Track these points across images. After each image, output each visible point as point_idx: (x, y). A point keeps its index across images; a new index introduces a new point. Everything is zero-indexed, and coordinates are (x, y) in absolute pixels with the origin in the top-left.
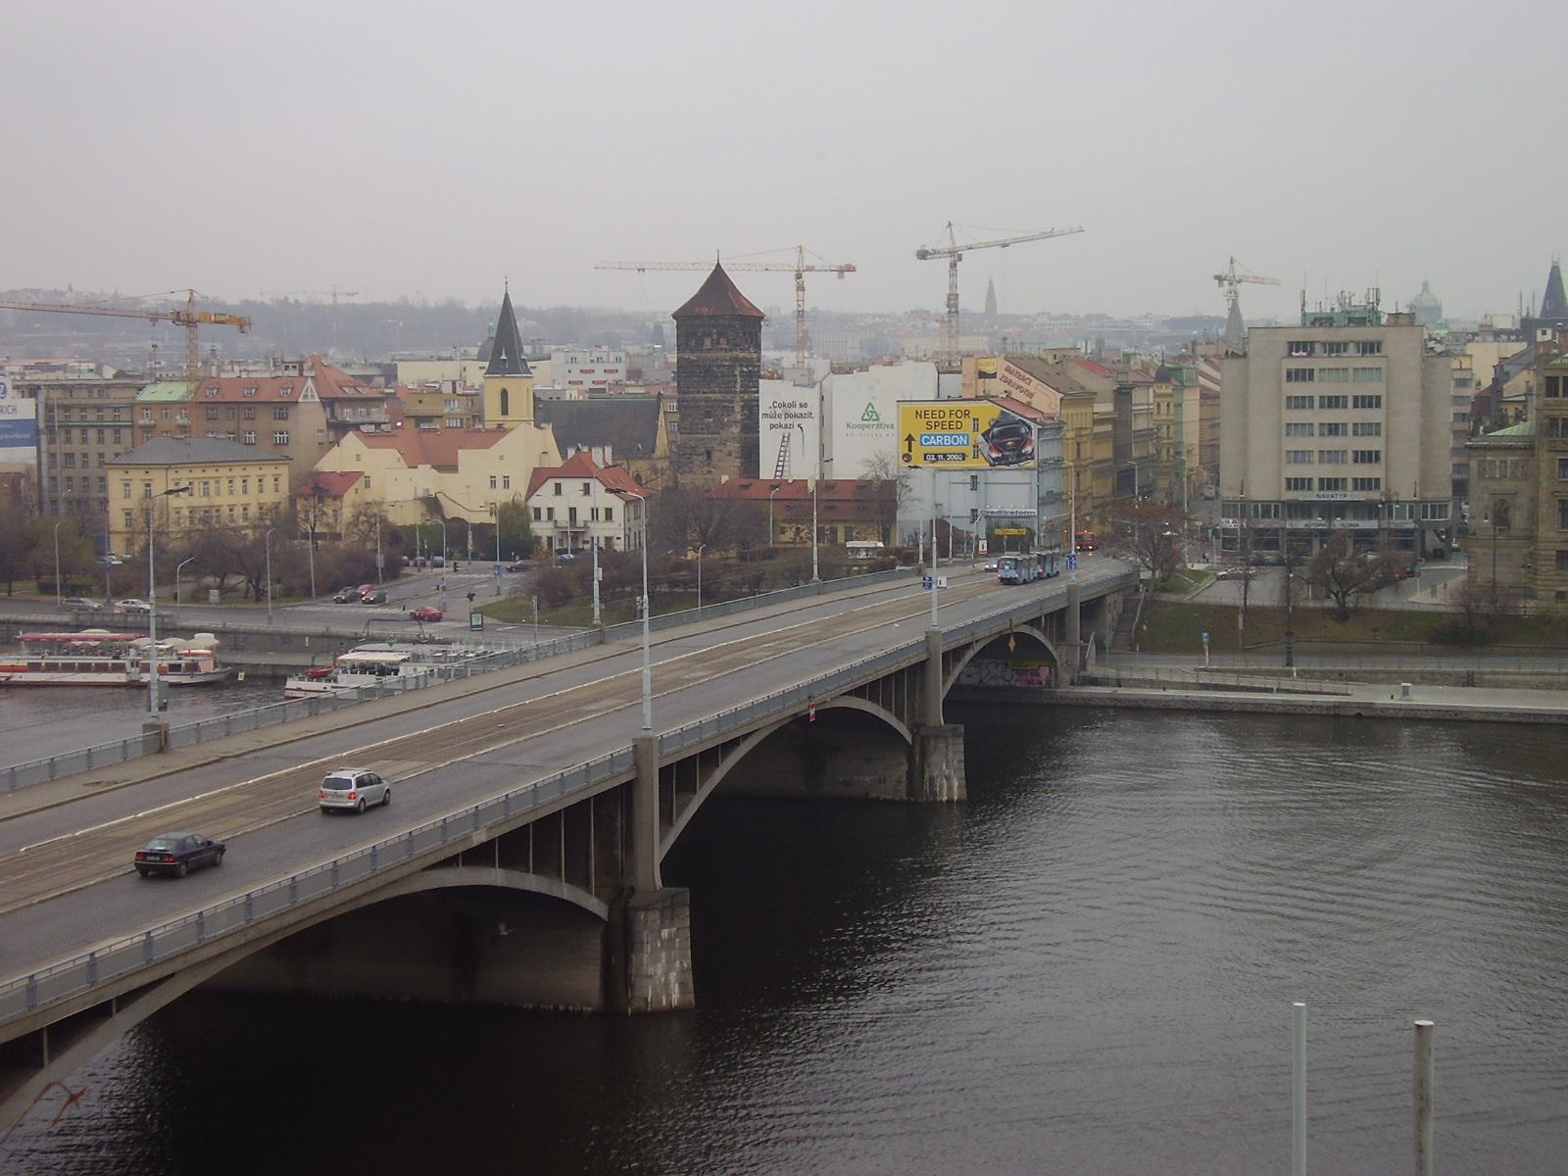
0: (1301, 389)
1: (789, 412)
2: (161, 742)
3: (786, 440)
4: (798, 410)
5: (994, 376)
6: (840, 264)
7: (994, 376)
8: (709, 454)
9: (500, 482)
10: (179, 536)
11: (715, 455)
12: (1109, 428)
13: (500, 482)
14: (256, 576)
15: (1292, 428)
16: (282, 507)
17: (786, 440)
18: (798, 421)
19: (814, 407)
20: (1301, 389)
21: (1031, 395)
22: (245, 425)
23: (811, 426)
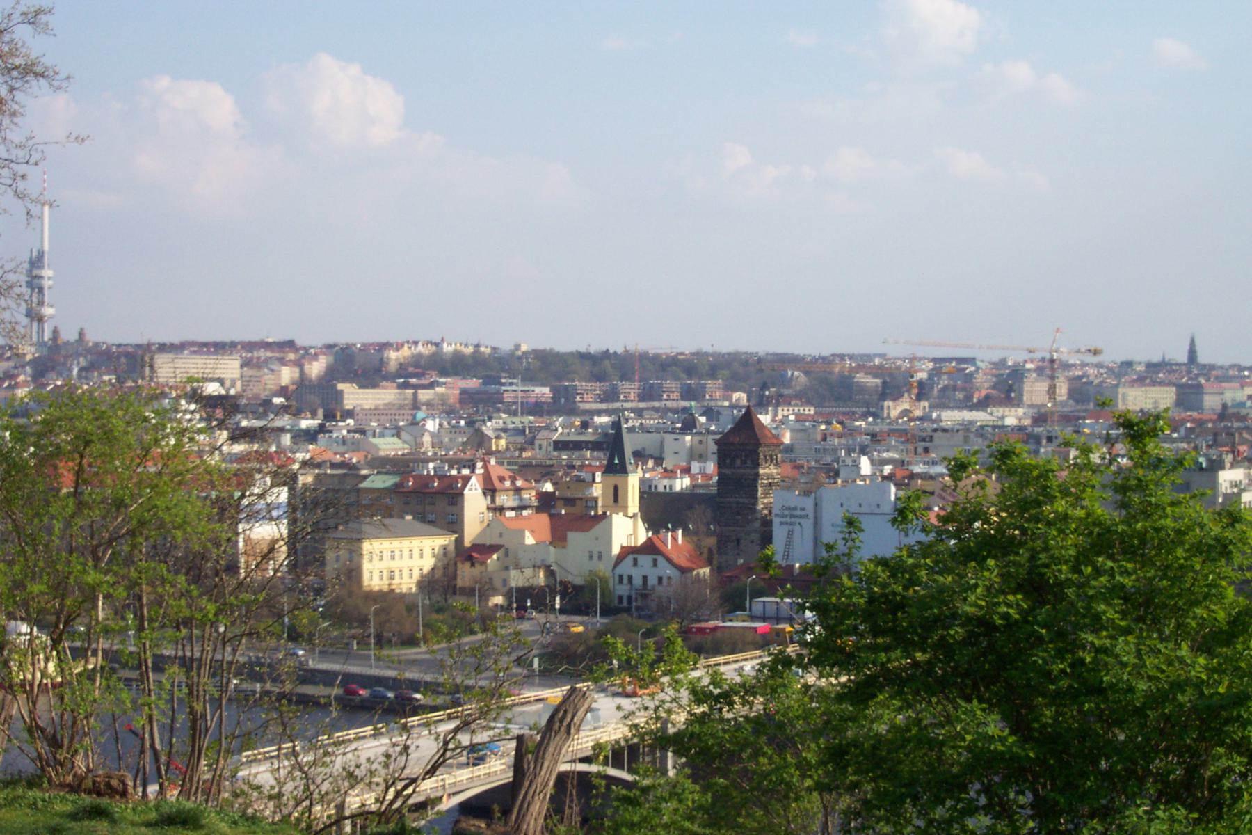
3: (790, 533)
4: (798, 512)
7: (932, 493)
8: (738, 541)
9: (595, 557)
13: (595, 557)
17: (790, 533)
18: (798, 520)
22: (428, 508)
23: (808, 524)
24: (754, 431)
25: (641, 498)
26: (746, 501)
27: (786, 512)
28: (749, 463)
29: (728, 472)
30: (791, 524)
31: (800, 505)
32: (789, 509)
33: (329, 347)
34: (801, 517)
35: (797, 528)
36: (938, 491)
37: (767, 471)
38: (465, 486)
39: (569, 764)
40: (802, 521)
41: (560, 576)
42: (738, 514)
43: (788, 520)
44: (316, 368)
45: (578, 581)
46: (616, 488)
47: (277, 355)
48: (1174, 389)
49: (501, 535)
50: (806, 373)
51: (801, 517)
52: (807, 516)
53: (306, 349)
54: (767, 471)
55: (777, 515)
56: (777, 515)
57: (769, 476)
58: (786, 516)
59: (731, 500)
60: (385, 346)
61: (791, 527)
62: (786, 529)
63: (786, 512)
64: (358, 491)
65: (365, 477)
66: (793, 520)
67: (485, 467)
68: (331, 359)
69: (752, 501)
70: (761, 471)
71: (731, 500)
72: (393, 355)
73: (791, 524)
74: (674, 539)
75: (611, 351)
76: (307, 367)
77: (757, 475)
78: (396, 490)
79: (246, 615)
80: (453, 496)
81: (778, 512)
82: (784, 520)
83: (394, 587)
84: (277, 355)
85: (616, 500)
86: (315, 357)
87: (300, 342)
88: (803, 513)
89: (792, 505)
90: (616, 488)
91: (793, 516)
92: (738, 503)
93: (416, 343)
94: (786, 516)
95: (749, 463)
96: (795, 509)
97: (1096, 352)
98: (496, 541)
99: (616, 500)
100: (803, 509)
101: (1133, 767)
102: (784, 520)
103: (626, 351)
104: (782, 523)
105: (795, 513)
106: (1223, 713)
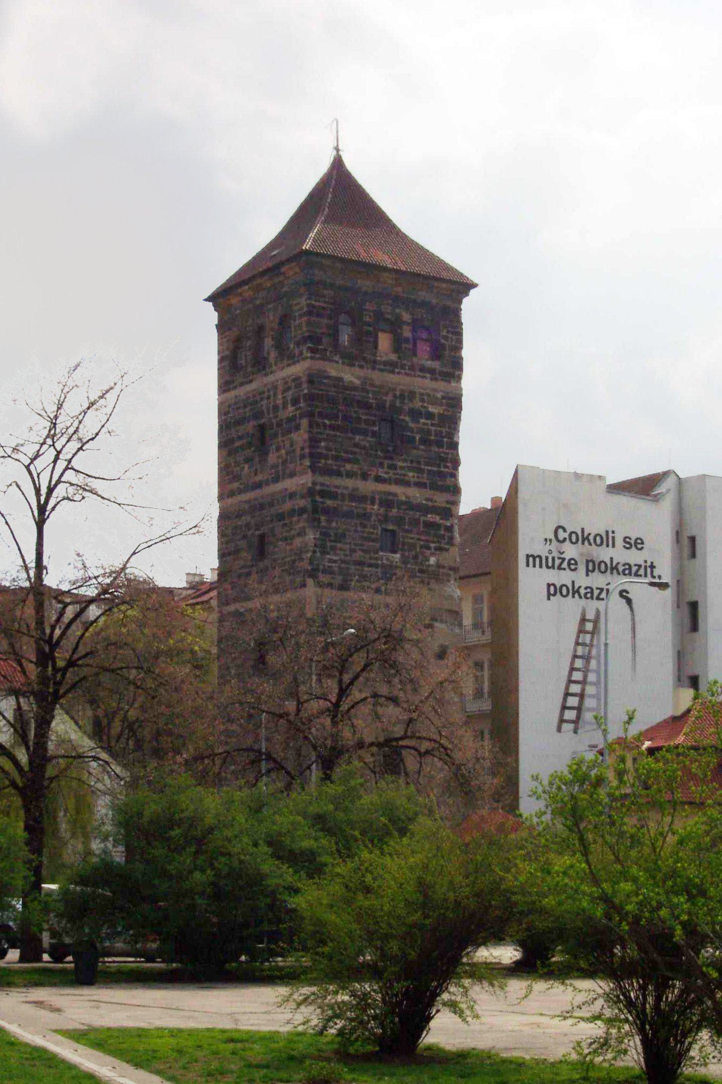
4: (619, 555)
18: (619, 582)
24: (404, 237)
26: (416, 495)
27: (571, 551)
30: (590, 594)
32: (584, 538)
34: (629, 570)
43: (582, 580)
47: (486, 690)
48: (44, 960)
51: (629, 570)
55: (533, 559)
56: (533, 559)
58: (572, 565)
59: (369, 487)
61: (592, 607)
63: (571, 551)
66: (598, 580)
69: (440, 499)
71: (369, 487)
73: (590, 594)
79: (565, 892)
81: (541, 550)
82: (564, 578)
83: (402, 781)
84: (486, 690)
88: (634, 557)
89: (595, 528)
91: (593, 566)
92: (388, 502)
94: (572, 565)
96: (606, 539)
100: (636, 544)
101: (384, 526)
102: (564, 578)
104: (553, 591)
105: (604, 554)
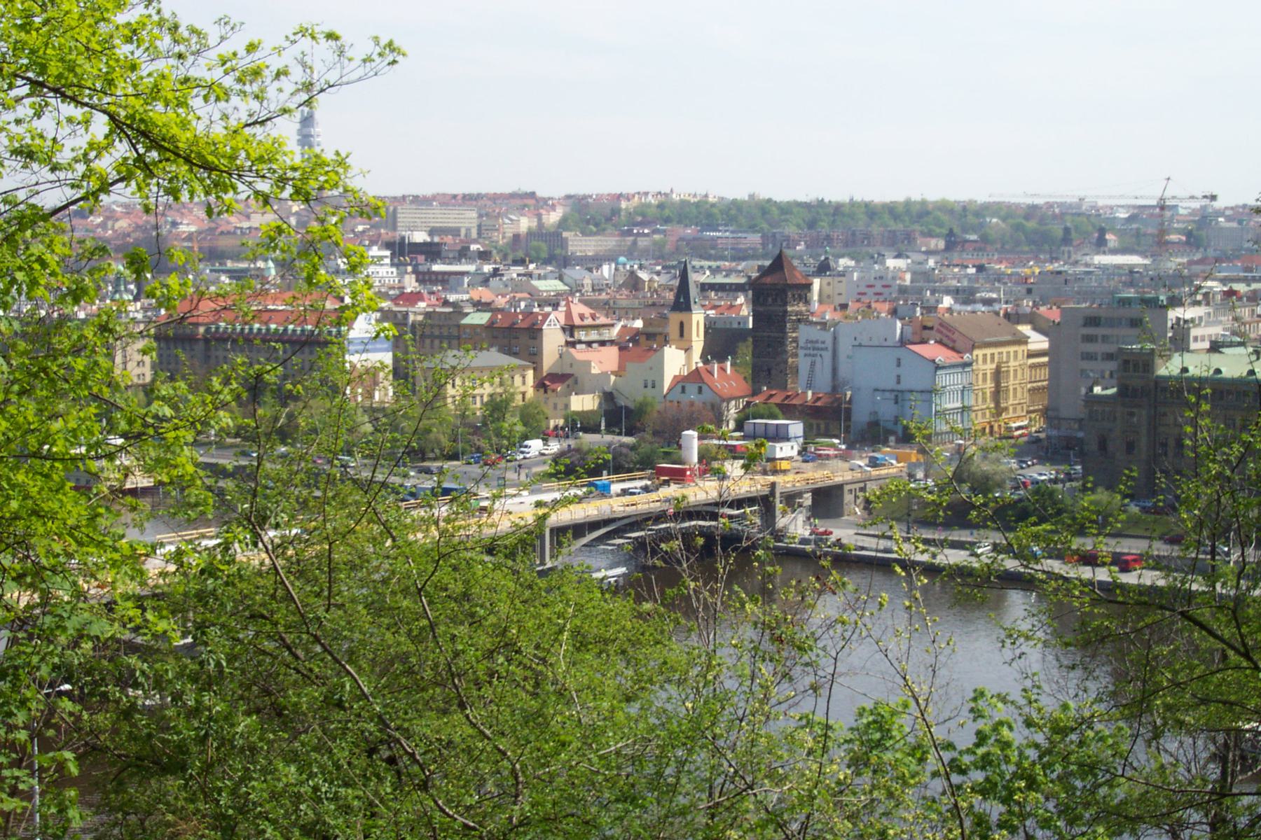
0: (1090, 348)
1: (814, 347)
2: (237, 257)
3: (813, 364)
4: (820, 345)
5: (931, 328)
6: (722, 195)
7: (931, 328)
8: (769, 370)
9: (650, 385)
10: (391, 292)
11: (773, 372)
12: (1045, 359)
13: (650, 385)
14: (234, 341)
15: (1033, 367)
16: (668, 247)
17: (813, 364)
18: (820, 352)
19: (829, 344)
20: (1090, 348)
21: (954, 341)
22: (513, 341)
23: (827, 355)
25: (706, 333)
28: (779, 302)
29: (761, 309)
30: (814, 356)
31: (821, 339)
32: (812, 342)
33: (568, 197)
35: (818, 359)
36: (936, 326)
37: (796, 308)
38: (543, 322)
39: (875, 540)
40: (823, 353)
41: (622, 402)
42: (769, 346)
44: (553, 218)
45: (631, 405)
46: (682, 324)
49: (571, 365)
50: (1004, 219)
52: (826, 349)
53: (545, 200)
54: (796, 308)
57: (797, 314)
60: (620, 196)
62: (809, 360)
64: (459, 326)
65: (467, 314)
67: (568, 305)
68: (568, 209)
70: (789, 309)
72: (624, 205)
73: (814, 356)
74: (723, 370)
75: (826, 200)
76: (544, 218)
77: (786, 311)
78: (490, 326)
80: (534, 332)
85: (682, 335)
86: (553, 207)
87: (540, 194)
90: (682, 324)
93: (646, 194)
95: (779, 302)
96: (817, 342)
97: (1213, 198)
98: (568, 371)
99: (682, 335)
103: (852, 200)
106: (663, 545)
